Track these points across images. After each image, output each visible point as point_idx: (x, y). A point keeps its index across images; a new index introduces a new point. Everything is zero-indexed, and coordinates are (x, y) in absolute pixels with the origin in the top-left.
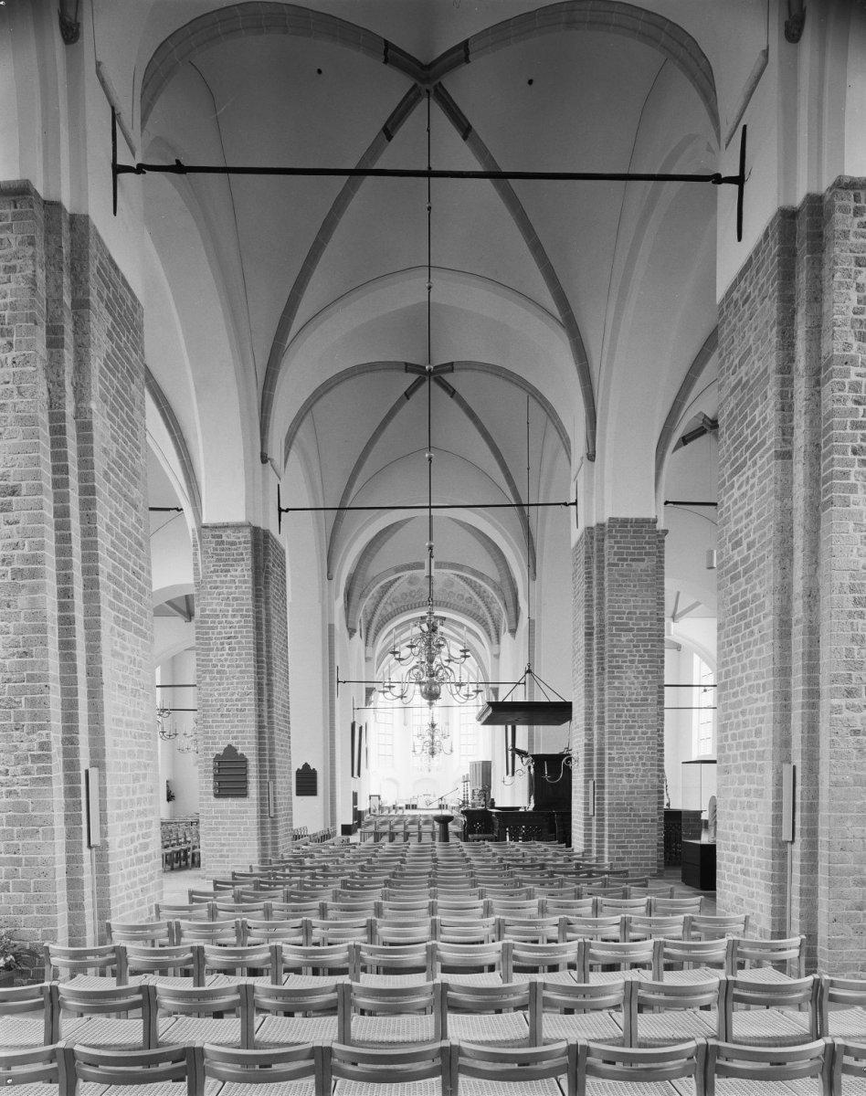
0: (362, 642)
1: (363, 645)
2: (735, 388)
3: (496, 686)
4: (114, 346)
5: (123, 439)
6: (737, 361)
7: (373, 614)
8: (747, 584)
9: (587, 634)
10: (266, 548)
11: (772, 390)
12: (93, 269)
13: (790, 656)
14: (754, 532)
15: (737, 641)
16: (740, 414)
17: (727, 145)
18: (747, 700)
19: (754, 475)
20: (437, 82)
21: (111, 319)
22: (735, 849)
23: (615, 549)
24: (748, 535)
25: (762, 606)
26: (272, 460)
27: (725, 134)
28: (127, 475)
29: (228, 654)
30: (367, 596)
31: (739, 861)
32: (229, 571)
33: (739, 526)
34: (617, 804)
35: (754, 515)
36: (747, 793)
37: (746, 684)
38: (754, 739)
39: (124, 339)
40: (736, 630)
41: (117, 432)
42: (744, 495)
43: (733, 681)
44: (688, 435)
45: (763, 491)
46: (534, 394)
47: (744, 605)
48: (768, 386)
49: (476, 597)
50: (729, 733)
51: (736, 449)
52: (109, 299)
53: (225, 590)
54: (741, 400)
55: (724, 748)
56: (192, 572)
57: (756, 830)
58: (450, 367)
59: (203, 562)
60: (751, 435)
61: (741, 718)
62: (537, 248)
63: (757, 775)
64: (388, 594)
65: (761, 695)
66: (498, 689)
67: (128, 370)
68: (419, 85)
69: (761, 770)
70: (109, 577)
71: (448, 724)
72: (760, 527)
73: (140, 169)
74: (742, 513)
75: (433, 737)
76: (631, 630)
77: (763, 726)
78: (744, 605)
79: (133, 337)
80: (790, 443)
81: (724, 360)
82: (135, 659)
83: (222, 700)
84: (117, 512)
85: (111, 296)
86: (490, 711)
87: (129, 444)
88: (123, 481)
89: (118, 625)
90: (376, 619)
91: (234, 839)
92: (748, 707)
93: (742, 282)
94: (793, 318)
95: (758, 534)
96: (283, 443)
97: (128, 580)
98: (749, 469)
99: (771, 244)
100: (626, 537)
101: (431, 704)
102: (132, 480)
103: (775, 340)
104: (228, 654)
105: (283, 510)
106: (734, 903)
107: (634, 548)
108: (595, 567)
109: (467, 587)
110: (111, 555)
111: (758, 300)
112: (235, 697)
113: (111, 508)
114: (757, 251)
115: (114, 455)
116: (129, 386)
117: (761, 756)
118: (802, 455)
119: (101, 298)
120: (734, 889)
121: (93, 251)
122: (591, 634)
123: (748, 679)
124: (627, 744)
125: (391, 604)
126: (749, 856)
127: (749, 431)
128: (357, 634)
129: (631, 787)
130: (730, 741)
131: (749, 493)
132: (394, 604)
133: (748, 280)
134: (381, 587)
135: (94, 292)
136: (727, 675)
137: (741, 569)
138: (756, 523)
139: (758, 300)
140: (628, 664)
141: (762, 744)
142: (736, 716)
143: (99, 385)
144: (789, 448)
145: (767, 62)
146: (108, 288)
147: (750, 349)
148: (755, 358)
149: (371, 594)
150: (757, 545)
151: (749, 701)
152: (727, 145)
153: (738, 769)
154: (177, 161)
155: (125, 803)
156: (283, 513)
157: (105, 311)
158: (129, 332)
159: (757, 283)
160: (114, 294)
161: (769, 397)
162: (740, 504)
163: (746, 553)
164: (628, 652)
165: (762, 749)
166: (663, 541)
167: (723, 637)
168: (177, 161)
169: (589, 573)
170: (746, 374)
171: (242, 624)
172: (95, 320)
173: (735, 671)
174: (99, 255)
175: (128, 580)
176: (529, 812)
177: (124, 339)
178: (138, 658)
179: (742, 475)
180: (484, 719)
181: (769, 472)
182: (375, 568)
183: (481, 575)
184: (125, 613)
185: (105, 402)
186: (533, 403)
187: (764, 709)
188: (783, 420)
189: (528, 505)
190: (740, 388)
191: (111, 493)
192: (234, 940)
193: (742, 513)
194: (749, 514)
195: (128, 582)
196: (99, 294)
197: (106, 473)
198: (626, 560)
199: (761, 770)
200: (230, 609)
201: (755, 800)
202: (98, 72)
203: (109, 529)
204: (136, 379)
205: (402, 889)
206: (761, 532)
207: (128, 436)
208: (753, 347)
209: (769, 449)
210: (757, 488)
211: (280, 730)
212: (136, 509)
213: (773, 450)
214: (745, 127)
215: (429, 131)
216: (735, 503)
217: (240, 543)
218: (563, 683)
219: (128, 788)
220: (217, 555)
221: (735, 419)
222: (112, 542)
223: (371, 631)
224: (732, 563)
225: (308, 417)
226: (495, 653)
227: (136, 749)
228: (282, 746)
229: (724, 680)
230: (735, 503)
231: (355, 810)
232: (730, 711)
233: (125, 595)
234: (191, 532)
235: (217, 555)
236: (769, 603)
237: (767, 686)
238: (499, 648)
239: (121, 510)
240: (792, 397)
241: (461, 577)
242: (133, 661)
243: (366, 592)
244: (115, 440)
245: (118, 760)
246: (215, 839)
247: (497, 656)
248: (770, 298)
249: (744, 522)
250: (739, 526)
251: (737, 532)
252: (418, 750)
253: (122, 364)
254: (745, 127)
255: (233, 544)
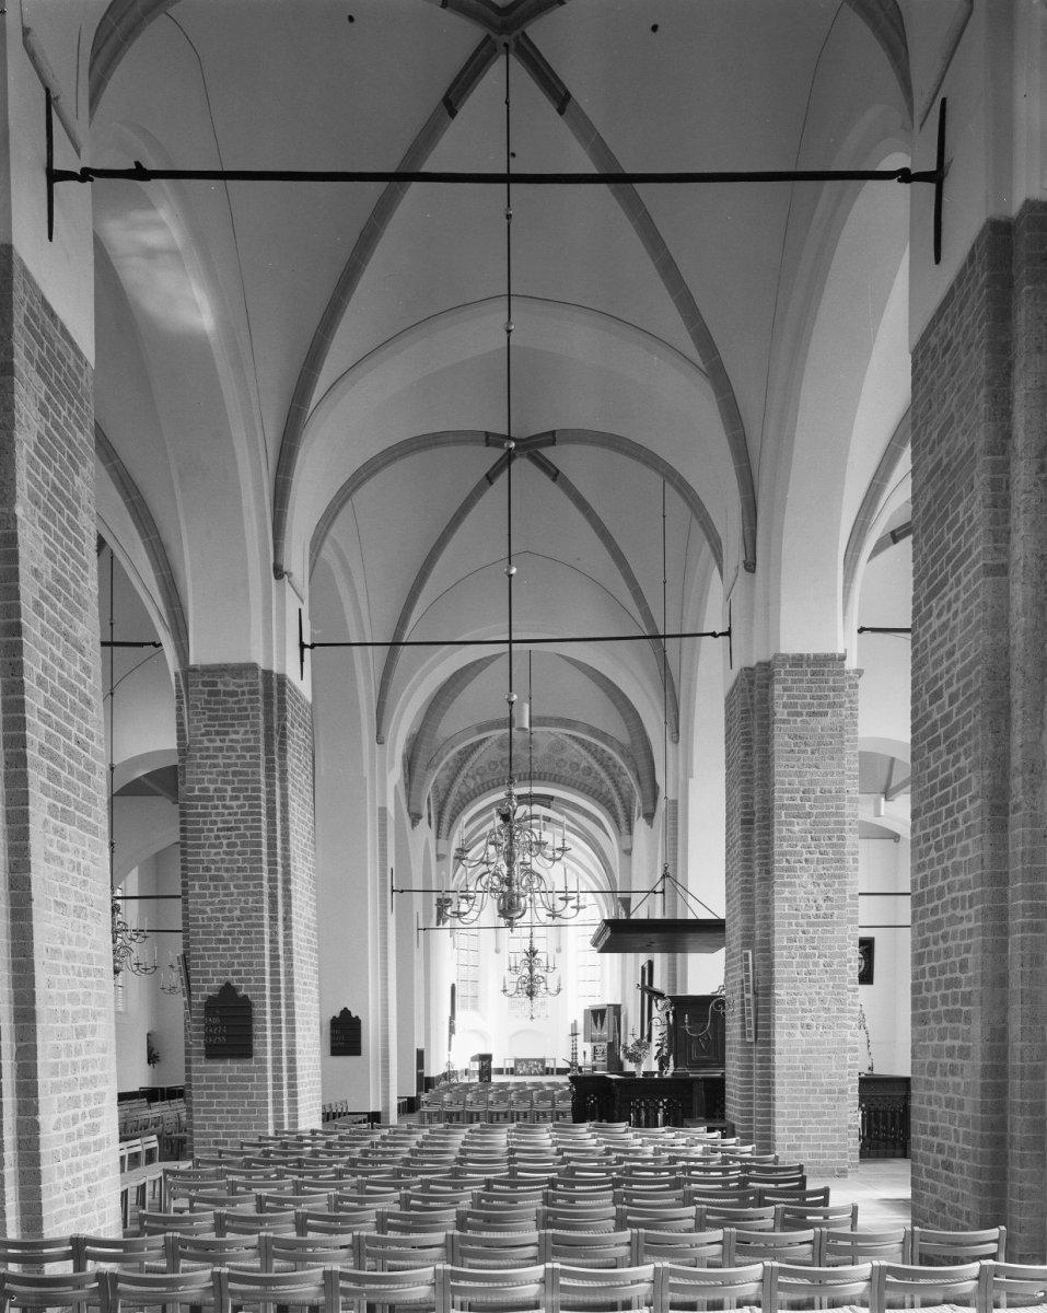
0: (432, 833)
1: (434, 837)
2: (933, 472)
3: (624, 895)
4: (49, 425)
5: (63, 556)
6: (935, 435)
7: (448, 792)
8: (948, 753)
9: (744, 822)
10: (282, 701)
11: (981, 477)
12: (18, 319)
13: (1006, 856)
14: (958, 680)
15: (936, 834)
16: (939, 510)
17: (922, 125)
18: (949, 919)
19: (957, 598)
20: (518, 32)
21: (45, 387)
22: (934, 1132)
23: (785, 699)
24: (949, 684)
25: (967, 784)
26: (290, 575)
27: (918, 114)
28: (68, 605)
29: (226, 853)
30: (436, 766)
31: (940, 1150)
32: (227, 733)
33: (939, 671)
34: (789, 1068)
35: (958, 655)
36: (950, 1052)
37: (948, 897)
38: (958, 974)
39: (64, 413)
40: (935, 820)
41: (53, 545)
42: (945, 626)
43: (931, 891)
44: (899, 529)
45: (968, 621)
46: (671, 476)
47: (946, 783)
48: (974, 473)
49: (596, 766)
50: (927, 966)
51: (935, 561)
52: (42, 359)
53: (220, 761)
54: (942, 489)
55: (921, 987)
56: (175, 734)
57: (961, 1106)
58: (551, 438)
59: (190, 721)
60: (954, 541)
61: (942, 945)
62: (668, 269)
63: (962, 1026)
64: (469, 764)
65: (967, 913)
66: (630, 899)
67: (70, 457)
68: (494, 36)
69: (968, 1019)
70: (42, 749)
71: (559, 950)
72: (965, 672)
73: (86, 175)
74: (943, 651)
75: (531, 970)
76: (809, 815)
77: (969, 956)
78: (946, 783)
79: (77, 409)
80: (1006, 552)
81: (918, 433)
82: (79, 864)
83: (217, 919)
84: (53, 658)
85: (44, 354)
86: (608, 934)
87: (72, 560)
88: (62, 614)
89: (56, 817)
90: (451, 799)
91: (233, 1119)
92: (950, 929)
93: (941, 324)
94: (1008, 375)
95: (962, 683)
96: (308, 547)
97: (71, 753)
98: (951, 590)
99: (978, 269)
100: (801, 681)
101: (511, 925)
102: (74, 611)
103: (983, 406)
104: (226, 853)
105: (307, 646)
106: (934, 1211)
107: (812, 698)
108: (756, 724)
109: (583, 752)
110: (45, 719)
111: (962, 348)
112: (237, 913)
113: (44, 653)
114: (960, 278)
115: (48, 577)
116: (72, 479)
117: (966, 999)
118: (1022, 571)
119: (31, 359)
120: (934, 1190)
121: (18, 294)
122: (751, 822)
123: (951, 888)
124: (802, 980)
125: (473, 778)
126: (952, 1143)
127: (951, 535)
128: (424, 821)
129: (808, 1043)
130: (928, 979)
131: (952, 623)
132: (478, 778)
133: (950, 319)
134: (459, 753)
135: (19, 350)
136: (924, 883)
137: (941, 731)
138: (959, 666)
139: (962, 348)
140: (804, 864)
141: (969, 981)
142: (936, 943)
143: (27, 481)
144: (1004, 560)
145: (972, 9)
146: (41, 343)
147: (952, 416)
148: (958, 431)
149: (442, 764)
150: (962, 699)
151: (953, 920)
152: (922, 125)
153: (937, 1017)
154: (137, 164)
155: (65, 1067)
156: (307, 651)
157: (36, 377)
158: (72, 404)
159: (961, 325)
160: (48, 351)
161: (976, 487)
162: (939, 639)
163: (947, 709)
164: (803, 847)
165: (968, 989)
166: (856, 686)
167: (918, 829)
168: (137, 164)
169: (747, 733)
170: (948, 453)
171: (246, 809)
172: (23, 391)
173: (934, 878)
174: (27, 299)
175: (71, 753)
176: (667, 1080)
177: (64, 413)
178: (84, 863)
179: (942, 598)
180: (601, 944)
181: (976, 594)
182: (448, 726)
183: (603, 736)
184: (66, 800)
185: (36, 503)
186: (670, 489)
187: (970, 931)
188: (995, 521)
189: (665, 636)
190: (939, 472)
191: (44, 632)
192: (257, 1264)
193: (943, 651)
194: (951, 653)
195: (70, 755)
196: (28, 354)
197: (37, 605)
198: (799, 714)
199: (968, 1019)
200: (229, 788)
201: (958, 1062)
202: (26, 44)
203: (41, 682)
204: (82, 470)
205: (634, 1205)
206: (965, 680)
207: (70, 550)
208: (956, 415)
209: (976, 562)
210: (961, 617)
211: (301, 961)
212: (81, 652)
213: (981, 563)
214: (944, 101)
215: (507, 103)
216: (933, 637)
217: (243, 693)
218: (707, 896)
219: (68, 1046)
220: (210, 710)
221: (933, 516)
222: (47, 701)
223: (444, 819)
224: (929, 723)
225: (347, 508)
226: (625, 847)
227: (81, 990)
228: (305, 984)
229: (920, 891)
230: (933, 637)
231: (420, 1076)
232: (927, 934)
233: (64, 774)
234: (173, 678)
235: (210, 710)
236: (977, 781)
237: (975, 900)
238: (631, 842)
239: (59, 654)
240: (1008, 488)
241: (574, 737)
242: (77, 867)
243: (435, 760)
244: (52, 557)
245: (54, 1008)
246: (207, 1119)
247: (628, 852)
248: (977, 346)
249: (946, 664)
250: (939, 671)
251: (936, 679)
252: (511, 989)
253: (61, 448)
254: (944, 101)
255: (233, 694)
